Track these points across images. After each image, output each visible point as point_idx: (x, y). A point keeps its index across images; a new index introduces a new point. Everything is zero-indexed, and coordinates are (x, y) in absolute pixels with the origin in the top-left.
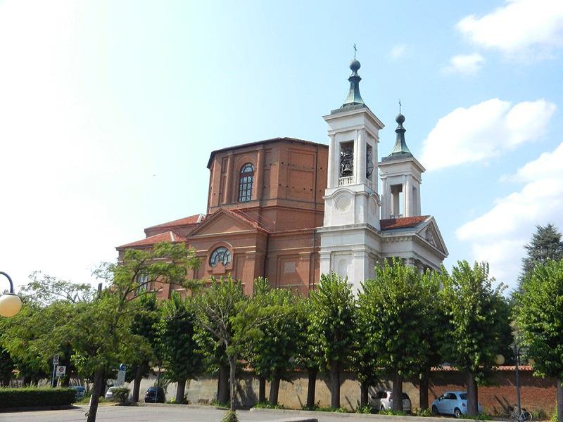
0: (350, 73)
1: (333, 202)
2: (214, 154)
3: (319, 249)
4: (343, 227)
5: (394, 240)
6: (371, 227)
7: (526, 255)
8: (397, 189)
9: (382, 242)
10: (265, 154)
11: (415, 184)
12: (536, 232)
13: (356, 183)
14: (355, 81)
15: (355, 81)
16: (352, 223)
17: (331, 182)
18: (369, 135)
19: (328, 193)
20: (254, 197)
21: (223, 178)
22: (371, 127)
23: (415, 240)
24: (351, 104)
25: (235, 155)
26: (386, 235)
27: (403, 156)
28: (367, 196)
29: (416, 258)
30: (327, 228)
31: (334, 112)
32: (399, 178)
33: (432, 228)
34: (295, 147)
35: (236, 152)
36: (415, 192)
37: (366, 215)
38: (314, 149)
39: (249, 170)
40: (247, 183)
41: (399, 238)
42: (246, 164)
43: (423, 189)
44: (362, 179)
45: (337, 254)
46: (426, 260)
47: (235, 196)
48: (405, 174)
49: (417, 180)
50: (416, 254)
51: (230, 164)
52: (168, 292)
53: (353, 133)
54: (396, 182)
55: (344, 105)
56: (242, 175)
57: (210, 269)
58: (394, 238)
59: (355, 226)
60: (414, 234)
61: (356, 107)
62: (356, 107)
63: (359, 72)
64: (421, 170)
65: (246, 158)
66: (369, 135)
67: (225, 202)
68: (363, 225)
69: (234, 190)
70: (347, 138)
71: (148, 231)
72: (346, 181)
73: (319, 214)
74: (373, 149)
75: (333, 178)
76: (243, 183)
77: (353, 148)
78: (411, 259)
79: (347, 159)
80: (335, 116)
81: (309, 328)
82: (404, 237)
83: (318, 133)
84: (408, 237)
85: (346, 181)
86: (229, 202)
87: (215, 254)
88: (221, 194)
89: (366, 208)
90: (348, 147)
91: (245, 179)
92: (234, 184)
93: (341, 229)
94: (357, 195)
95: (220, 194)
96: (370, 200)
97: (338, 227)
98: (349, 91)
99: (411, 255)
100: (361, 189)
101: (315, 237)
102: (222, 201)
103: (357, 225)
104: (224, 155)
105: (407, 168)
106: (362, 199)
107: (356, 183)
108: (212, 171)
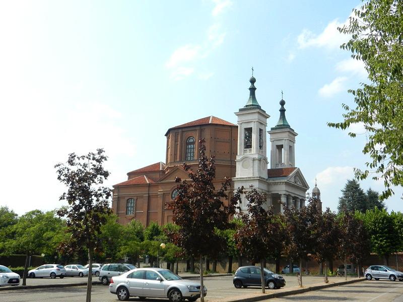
0: (250, 85)
1: (241, 163)
2: (170, 131)
4: (246, 178)
5: (276, 184)
6: (262, 178)
7: (341, 195)
8: (280, 147)
9: (269, 185)
10: (201, 131)
11: (291, 144)
12: (347, 182)
13: (254, 152)
14: (253, 90)
15: (253, 90)
16: (251, 176)
17: (239, 152)
18: (261, 123)
19: (238, 158)
20: (196, 158)
21: (176, 146)
22: (262, 119)
23: (287, 184)
24: (250, 105)
25: (183, 132)
26: (271, 181)
27: (283, 126)
28: (260, 160)
29: (287, 193)
30: (238, 178)
31: (241, 110)
33: (299, 175)
34: (217, 127)
35: (184, 130)
36: (291, 149)
37: (259, 171)
38: (230, 128)
39: (191, 141)
40: (191, 149)
41: (278, 182)
42: (189, 138)
43: (297, 146)
44: (256, 150)
46: (294, 194)
47: (184, 157)
48: (285, 139)
49: (293, 141)
50: (287, 191)
51: (180, 139)
52: (146, 213)
53: (252, 123)
54: (280, 143)
55: (247, 106)
56: (188, 144)
58: (275, 183)
59: (253, 178)
61: (254, 107)
62: (254, 107)
63: (255, 84)
64: (295, 135)
65: (190, 134)
66: (261, 123)
67: (178, 160)
68: (257, 177)
69: (183, 152)
70: (248, 126)
71: (130, 174)
72: (248, 151)
73: (233, 168)
74: (264, 131)
75: (240, 149)
76: (188, 149)
77: (252, 131)
78: (284, 194)
79: (248, 138)
80: (243, 111)
81: (229, 240)
82: (280, 182)
83: (233, 120)
84: (283, 182)
85: (248, 151)
86: (181, 160)
88: (175, 155)
89: (259, 167)
90: (249, 130)
91: (190, 146)
92: (183, 152)
94: (254, 160)
95: (175, 154)
96: (261, 162)
97: (244, 178)
98: (249, 96)
99: (284, 193)
100: (256, 156)
102: (177, 159)
103: (254, 177)
104: (176, 131)
105: (285, 136)
106: (256, 162)
107: (254, 152)
108: (168, 138)
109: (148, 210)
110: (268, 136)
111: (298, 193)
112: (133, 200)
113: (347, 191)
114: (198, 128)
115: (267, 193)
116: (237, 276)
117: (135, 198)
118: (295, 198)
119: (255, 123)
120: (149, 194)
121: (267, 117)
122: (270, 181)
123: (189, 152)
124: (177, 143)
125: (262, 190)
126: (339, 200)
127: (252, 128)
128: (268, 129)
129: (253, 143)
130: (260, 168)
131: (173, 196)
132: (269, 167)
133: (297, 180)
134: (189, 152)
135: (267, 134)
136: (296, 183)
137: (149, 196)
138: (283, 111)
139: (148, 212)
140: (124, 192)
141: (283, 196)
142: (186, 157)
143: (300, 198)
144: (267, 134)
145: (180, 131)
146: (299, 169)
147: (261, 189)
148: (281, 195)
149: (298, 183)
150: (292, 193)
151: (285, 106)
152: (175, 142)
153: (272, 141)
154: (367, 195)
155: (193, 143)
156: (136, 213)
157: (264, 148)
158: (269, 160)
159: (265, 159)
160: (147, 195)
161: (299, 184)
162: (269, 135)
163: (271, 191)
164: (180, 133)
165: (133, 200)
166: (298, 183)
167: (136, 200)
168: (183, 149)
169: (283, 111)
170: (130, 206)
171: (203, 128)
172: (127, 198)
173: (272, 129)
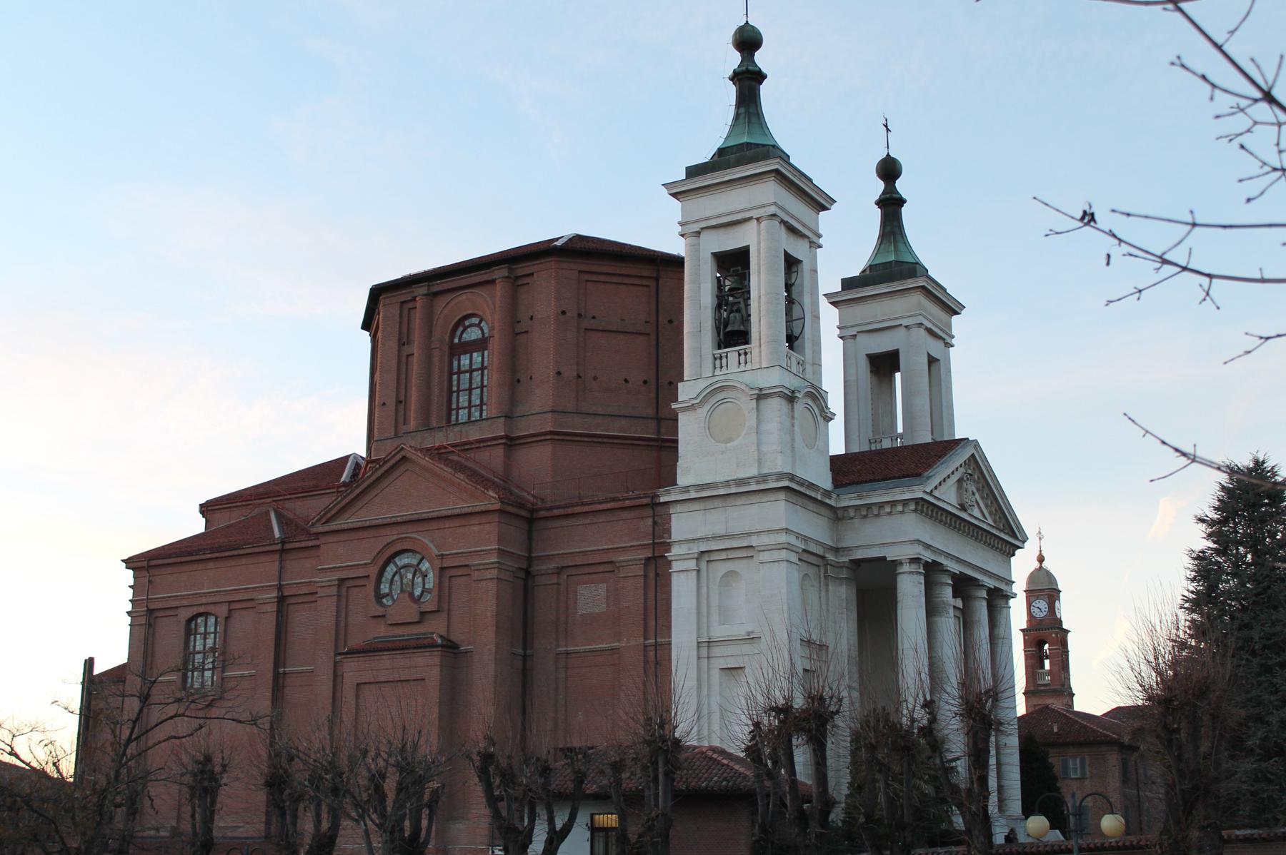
2: (378, 293)
3: (668, 546)
5: (868, 511)
6: (802, 482)
7: (1200, 540)
9: (838, 516)
10: (516, 283)
11: (935, 348)
16: (752, 471)
18: (792, 230)
19: (686, 392)
22: (798, 209)
26: (848, 500)
29: (928, 556)
30: (686, 489)
31: (693, 172)
32: (741, 230)
39: (473, 334)
40: (471, 371)
41: (881, 505)
52: (270, 676)
57: (380, 611)
58: (869, 507)
60: (919, 495)
64: (952, 308)
65: (465, 302)
66: (792, 230)
67: (412, 424)
69: (436, 390)
70: (729, 241)
71: (207, 509)
78: (915, 560)
84: (905, 502)
87: (391, 569)
91: (465, 360)
93: (722, 491)
94: (761, 396)
101: (658, 514)
104: (404, 295)
105: (907, 306)
109: (277, 665)
110: (829, 318)
111: (974, 557)
112: (212, 620)
113: (1223, 522)
114: (500, 273)
115: (830, 556)
116: (902, 785)
117: (222, 611)
118: (963, 585)
119: (764, 224)
120: (280, 588)
121: (820, 203)
122: (844, 503)
123: (465, 385)
124: (406, 350)
125: (806, 539)
126: (1189, 563)
127: (748, 246)
128: (829, 282)
129: (754, 319)
130: (792, 433)
131: (385, 588)
132: (837, 446)
133: (968, 499)
134: (465, 385)
135: (824, 305)
136: (963, 508)
137: (282, 600)
138: (891, 205)
139: (276, 675)
140: (175, 586)
141: (906, 568)
142: (450, 410)
143: (990, 583)
144: (824, 305)
145: (421, 290)
146: (976, 444)
147: (798, 535)
148: (896, 564)
149: (976, 513)
150: (948, 555)
151: (901, 185)
152: (401, 344)
153: (848, 335)
154: (840, 824)
155: (481, 345)
156: (223, 679)
157: (808, 345)
158: (836, 403)
159: (817, 396)
160: (275, 594)
161: (978, 514)
162: (834, 312)
163: (848, 549)
164: (420, 303)
165: (212, 620)
166: (976, 513)
167: (227, 618)
168: (436, 375)
169: (891, 205)
170: (199, 647)
171: (522, 269)
172: (184, 614)
173: (848, 284)
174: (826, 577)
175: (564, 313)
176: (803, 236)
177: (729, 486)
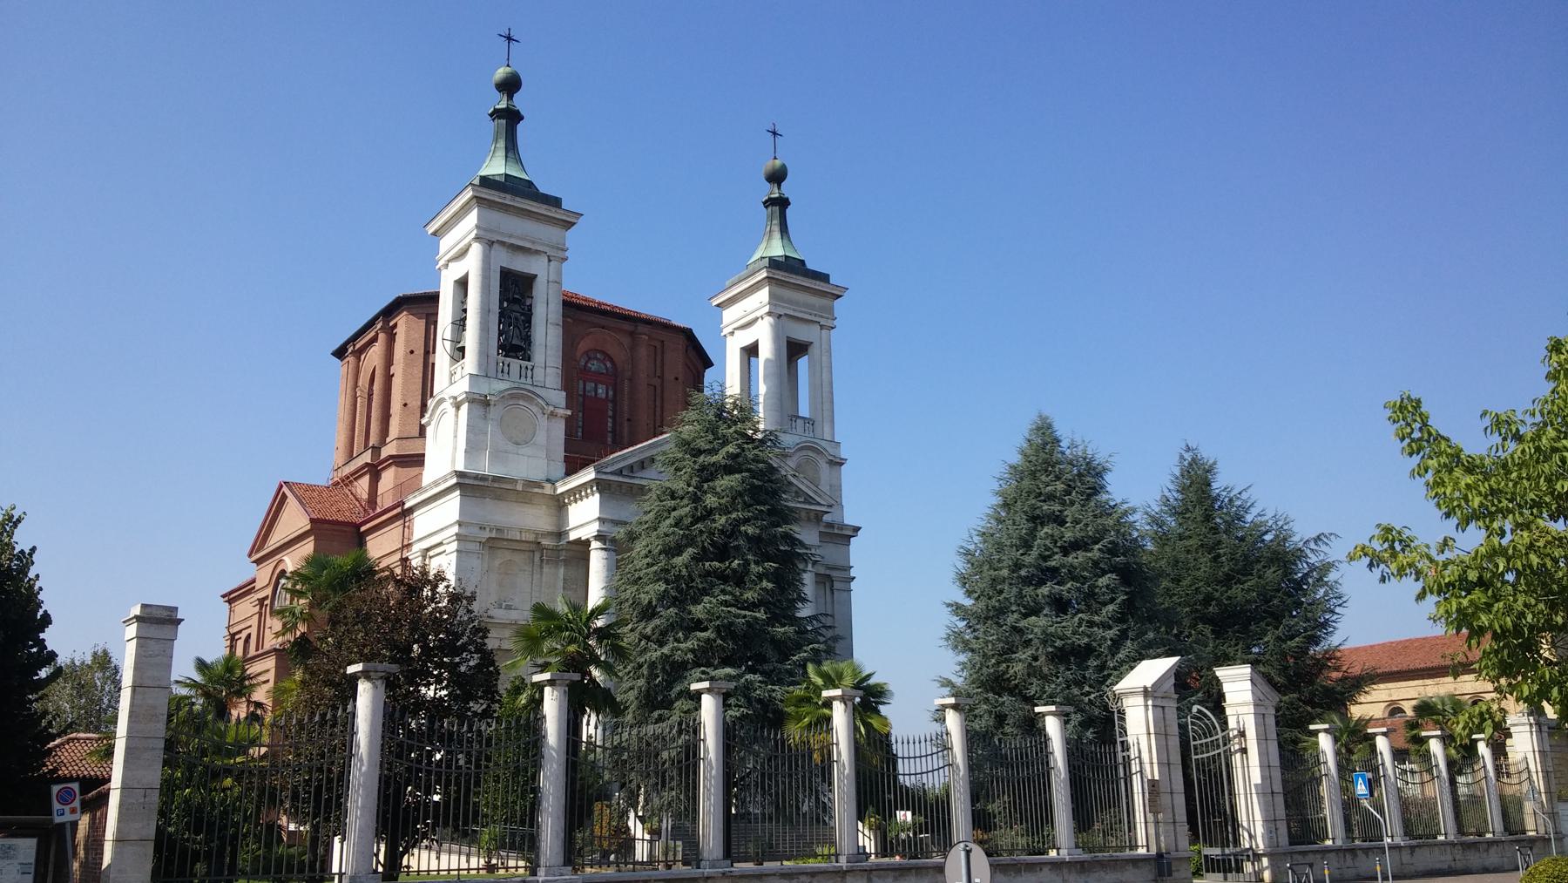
45: (431, 553)
148: (587, 543)
174: (542, 561)
175: (412, 352)
176: (537, 252)
177: (446, 480)
